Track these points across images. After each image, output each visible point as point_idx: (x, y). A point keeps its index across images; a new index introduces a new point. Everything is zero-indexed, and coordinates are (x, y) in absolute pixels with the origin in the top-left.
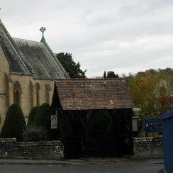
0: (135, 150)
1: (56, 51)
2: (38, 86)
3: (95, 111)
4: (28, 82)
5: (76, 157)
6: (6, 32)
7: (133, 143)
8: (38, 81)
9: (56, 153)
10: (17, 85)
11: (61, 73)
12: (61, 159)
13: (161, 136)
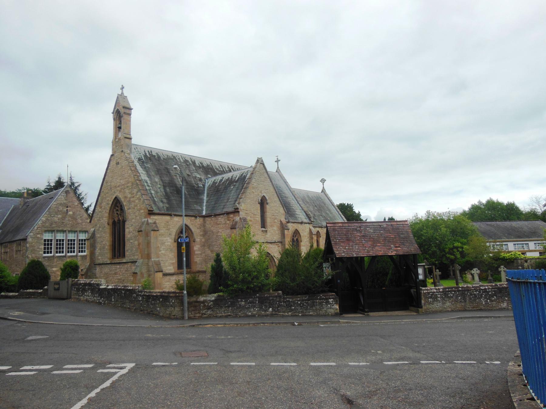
0: (423, 302)
1: (337, 202)
2: (318, 234)
3: (373, 258)
4: (308, 230)
5: (355, 311)
6: (286, 182)
7: (420, 293)
8: (318, 229)
9: (330, 310)
10: (296, 233)
11: (340, 218)
12: (336, 315)
13: (98, 225)
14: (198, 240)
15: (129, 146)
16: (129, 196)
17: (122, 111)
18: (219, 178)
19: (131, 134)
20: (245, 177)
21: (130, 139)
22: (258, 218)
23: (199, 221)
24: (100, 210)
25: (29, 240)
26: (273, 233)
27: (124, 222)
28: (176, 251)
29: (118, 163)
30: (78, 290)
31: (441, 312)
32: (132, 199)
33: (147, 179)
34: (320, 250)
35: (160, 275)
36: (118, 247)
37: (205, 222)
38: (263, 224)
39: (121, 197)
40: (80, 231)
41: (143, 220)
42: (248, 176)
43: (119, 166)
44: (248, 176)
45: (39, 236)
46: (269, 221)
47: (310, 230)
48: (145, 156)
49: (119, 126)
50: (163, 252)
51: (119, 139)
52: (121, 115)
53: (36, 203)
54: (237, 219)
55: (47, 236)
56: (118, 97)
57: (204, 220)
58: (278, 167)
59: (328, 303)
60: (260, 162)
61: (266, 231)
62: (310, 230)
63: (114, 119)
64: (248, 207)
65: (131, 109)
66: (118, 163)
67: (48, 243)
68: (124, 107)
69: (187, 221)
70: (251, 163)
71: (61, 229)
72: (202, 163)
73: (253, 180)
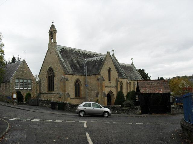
0: (171, 110)
1: (138, 68)
2: (130, 83)
4: (126, 82)
6: (117, 60)
8: (130, 81)
10: (121, 83)
11: (140, 78)
14: (82, 85)
15: (56, 46)
16: (56, 66)
17: (53, 32)
18: (91, 59)
19: (57, 41)
20: (102, 60)
21: (56, 43)
22: (108, 77)
23: (83, 77)
24: (43, 71)
25: (11, 82)
26: (113, 83)
27: (54, 77)
28: (74, 89)
29: (51, 53)
30: (42, 102)
31: (177, 114)
32: (57, 68)
33: (63, 59)
34: (134, 91)
35: (69, 98)
36: (51, 87)
37: (85, 77)
38: (110, 79)
39: (52, 67)
40: (29, 79)
41: (62, 77)
42: (103, 59)
43: (52, 54)
44: (103, 59)
45: (14, 80)
46: (112, 78)
47: (127, 81)
48: (61, 50)
49: (52, 38)
50: (70, 89)
51: (52, 43)
52: (53, 32)
53: (11, 67)
54: (99, 77)
55: (17, 81)
56: (51, 26)
57: (85, 77)
58: (113, 54)
59: (137, 110)
60: (108, 53)
61: (111, 82)
62: (127, 81)
63: (50, 35)
64: (104, 72)
65: (56, 31)
66: (51, 53)
67: (17, 83)
68: (54, 30)
69: (78, 77)
70: (105, 53)
71: (21, 78)
72: (82, 53)
73: (106, 61)
